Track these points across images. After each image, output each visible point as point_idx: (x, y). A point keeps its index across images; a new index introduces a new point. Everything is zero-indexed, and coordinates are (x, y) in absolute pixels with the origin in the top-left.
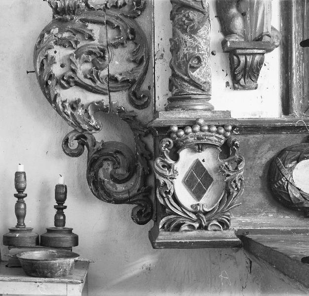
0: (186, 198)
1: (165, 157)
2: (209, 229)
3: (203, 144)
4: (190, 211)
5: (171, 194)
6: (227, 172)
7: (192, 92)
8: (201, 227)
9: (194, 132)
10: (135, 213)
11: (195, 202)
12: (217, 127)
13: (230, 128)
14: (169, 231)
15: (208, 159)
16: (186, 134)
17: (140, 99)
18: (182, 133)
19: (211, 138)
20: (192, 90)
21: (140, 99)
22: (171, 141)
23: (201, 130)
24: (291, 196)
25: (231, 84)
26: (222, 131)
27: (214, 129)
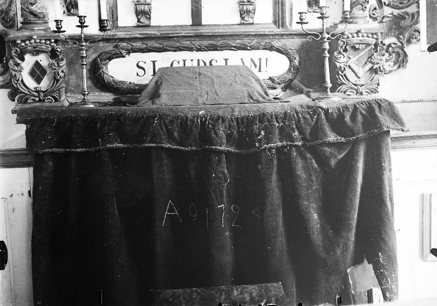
0: (31, 83)
1: (14, 59)
2: (46, 101)
3: (38, 51)
4: (33, 91)
5: (20, 80)
6: (54, 68)
7: (32, 19)
8: (40, 101)
9: (30, 43)
10: (10, 94)
11: (391, 137)
12: (45, 40)
13: (53, 41)
14: (21, 103)
15: (44, 60)
16: (26, 44)
17: (7, 22)
18: (23, 44)
19: (42, 47)
20: (32, 18)
21: (7, 22)
22: (18, 50)
23: (35, 42)
24: (106, 81)
25: (66, 12)
26: (48, 42)
27: (43, 41)
